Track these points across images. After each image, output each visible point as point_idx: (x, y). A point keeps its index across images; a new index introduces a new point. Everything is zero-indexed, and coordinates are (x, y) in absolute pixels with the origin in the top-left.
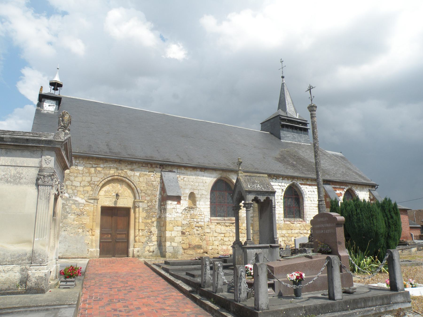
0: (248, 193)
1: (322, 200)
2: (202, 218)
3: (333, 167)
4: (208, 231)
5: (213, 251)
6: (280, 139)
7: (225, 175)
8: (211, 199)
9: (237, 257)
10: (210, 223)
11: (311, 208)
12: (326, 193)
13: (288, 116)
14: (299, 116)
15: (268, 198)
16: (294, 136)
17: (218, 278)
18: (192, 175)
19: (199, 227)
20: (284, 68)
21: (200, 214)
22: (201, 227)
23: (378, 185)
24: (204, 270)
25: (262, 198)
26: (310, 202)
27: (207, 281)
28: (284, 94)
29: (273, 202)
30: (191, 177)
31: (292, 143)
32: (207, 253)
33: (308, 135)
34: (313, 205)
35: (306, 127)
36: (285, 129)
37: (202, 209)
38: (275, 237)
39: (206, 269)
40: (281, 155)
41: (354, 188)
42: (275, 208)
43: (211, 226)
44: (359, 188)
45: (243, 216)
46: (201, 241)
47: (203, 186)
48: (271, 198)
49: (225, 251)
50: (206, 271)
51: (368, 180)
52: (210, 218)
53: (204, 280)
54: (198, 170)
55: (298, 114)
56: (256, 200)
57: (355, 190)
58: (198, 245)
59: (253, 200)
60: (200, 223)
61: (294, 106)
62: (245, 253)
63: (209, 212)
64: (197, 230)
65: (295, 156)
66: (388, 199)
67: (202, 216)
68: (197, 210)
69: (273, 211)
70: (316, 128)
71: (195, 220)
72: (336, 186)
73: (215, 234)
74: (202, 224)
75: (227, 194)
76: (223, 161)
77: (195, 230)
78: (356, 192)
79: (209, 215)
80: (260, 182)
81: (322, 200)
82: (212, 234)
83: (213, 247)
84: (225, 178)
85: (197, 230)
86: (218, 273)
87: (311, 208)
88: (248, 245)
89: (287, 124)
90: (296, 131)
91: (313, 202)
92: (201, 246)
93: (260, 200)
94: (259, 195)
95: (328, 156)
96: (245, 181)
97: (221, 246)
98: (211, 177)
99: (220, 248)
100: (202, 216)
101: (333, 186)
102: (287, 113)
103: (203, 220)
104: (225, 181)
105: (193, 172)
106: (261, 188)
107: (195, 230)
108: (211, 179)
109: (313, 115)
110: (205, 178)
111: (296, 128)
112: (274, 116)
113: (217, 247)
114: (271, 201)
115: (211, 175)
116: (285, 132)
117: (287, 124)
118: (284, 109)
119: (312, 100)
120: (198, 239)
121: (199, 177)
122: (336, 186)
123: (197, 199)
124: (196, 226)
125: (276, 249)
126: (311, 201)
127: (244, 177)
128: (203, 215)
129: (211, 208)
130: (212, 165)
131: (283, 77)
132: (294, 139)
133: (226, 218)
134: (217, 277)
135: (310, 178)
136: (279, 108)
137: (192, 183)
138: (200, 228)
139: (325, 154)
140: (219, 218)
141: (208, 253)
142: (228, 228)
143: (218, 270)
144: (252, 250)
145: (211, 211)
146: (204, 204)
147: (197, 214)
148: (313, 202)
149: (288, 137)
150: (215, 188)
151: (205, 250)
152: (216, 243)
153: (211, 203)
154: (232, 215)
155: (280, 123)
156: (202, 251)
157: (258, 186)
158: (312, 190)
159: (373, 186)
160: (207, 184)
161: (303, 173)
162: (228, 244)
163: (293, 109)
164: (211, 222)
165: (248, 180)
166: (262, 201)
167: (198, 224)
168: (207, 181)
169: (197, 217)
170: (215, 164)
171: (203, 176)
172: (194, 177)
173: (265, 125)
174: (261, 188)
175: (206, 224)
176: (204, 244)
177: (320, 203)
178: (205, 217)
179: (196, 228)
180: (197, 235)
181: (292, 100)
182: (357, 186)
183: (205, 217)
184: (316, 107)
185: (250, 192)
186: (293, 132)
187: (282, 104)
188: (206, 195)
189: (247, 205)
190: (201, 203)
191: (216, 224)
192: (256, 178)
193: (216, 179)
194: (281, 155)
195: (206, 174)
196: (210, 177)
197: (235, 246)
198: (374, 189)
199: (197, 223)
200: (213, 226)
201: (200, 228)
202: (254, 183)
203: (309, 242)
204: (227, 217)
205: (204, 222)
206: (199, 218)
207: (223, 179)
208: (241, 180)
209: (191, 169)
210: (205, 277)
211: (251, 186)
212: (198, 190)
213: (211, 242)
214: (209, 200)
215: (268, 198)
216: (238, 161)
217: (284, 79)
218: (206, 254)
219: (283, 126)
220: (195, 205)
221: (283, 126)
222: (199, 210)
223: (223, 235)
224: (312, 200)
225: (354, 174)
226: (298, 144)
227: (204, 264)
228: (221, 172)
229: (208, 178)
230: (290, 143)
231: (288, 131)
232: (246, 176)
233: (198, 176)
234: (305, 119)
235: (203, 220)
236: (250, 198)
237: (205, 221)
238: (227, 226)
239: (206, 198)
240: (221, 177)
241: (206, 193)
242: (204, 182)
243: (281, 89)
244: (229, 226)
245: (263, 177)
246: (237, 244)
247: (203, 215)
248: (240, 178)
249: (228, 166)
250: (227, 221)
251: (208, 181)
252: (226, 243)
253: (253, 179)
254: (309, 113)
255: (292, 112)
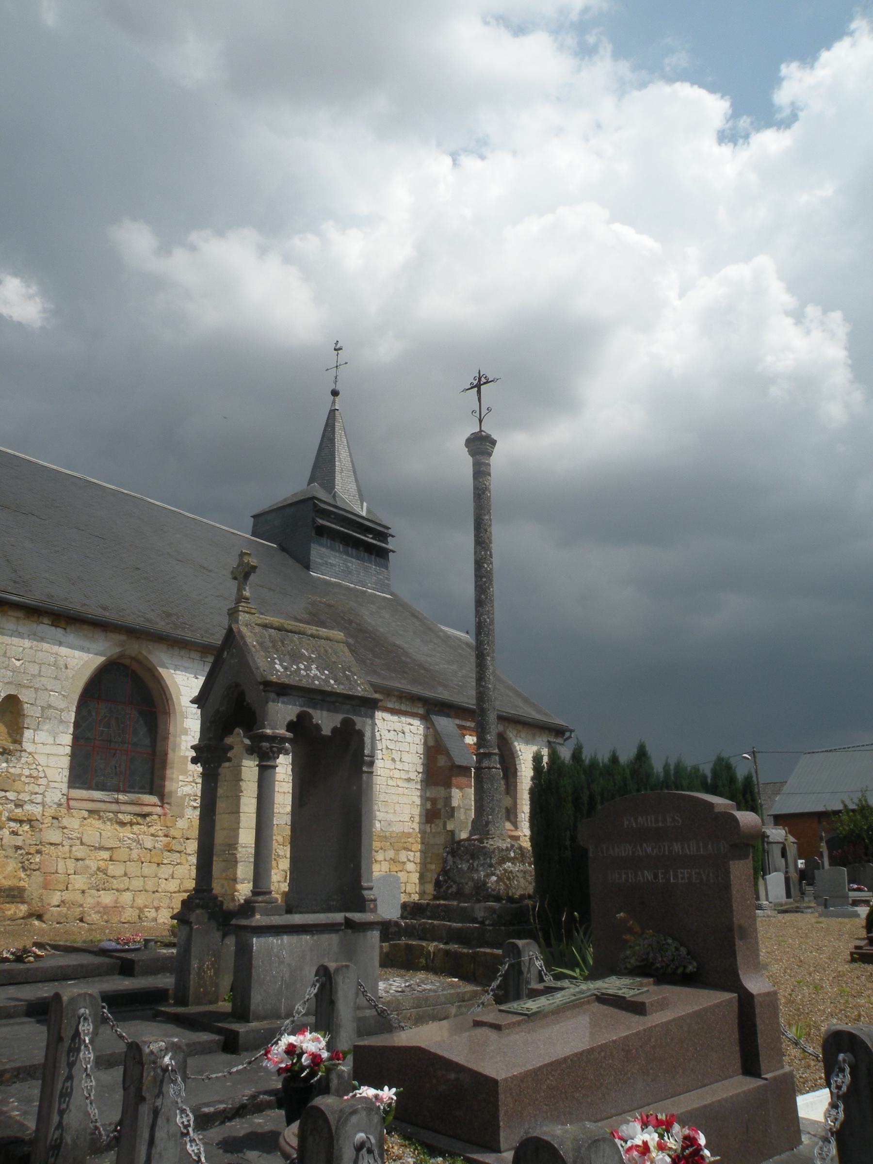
0: (273, 695)
1: (488, 755)
2: (37, 789)
3: (455, 667)
4: (54, 836)
5: (64, 910)
6: (307, 567)
7: (134, 648)
8: (76, 725)
9: (195, 964)
10: (64, 811)
11: (390, 782)
12: (436, 741)
13: (339, 504)
14: (368, 511)
15: (348, 724)
16: (348, 567)
17: (151, 1143)
18: (21, 635)
19: (21, 822)
20: (341, 368)
21: (30, 776)
22: (30, 821)
23: (571, 731)
24: (63, 1072)
25: (326, 721)
26: (389, 764)
27: (68, 1139)
28: (332, 441)
29: (367, 740)
30: (15, 640)
31: (339, 585)
32: (40, 917)
33: (387, 568)
34: (397, 774)
35: (384, 545)
36: (324, 540)
37: (42, 760)
38: (364, 884)
39: (71, 1065)
40: (310, 613)
41: (511, 734)
42: (371, 764)
43: (65, 822)
44: (523, 735)
45: (179, 794)
46: (23, 875)
47: (56, 678)
48: (359, 722)
49: (106, 910)
50: (70, 1078)
51: (546, 715)
52: (65, 791)
53: (53, 1134)
54: (46, 621)
55: (365, 504)
56: (300, 727)
57: (513, 738)
58: (11, 889)
59: (291, 726)
60: (27, 807)
61: (356, 480)
62: (244, 953)
63: (66, 772)
64: (15, 833)
65: (350, 622)
66: (672, 767)
67: (41, 781)
68: (23, 760)
69: (365, 777)
70: (489, 512)
71: (11, 795)
72: (464, 723)
73: (79, 851)
74: (37, 810)
75: (135, 714)
76: (132, 604)
77: (6, 832)
78: (516, 744)
79: (66, 780)
80: (319, 656)
81: (488, 755)
82: (67, 848)
83: (66, 896)
84: (132, 658)
85: (15, 833)
86: (156, 1112)
87: (390, 782)
88: (258, 919)
89: (334, 526)
90: (354, 551)
91: (399, 765)
92: (21, 890)
93: (318, 727)
94: (314, 707)
95: (438, 637)
96: (261, 644)
97: (94, 892)
98: (88, 651)
99: (89, 901)
100: (41, 781)
101: (458, 722)
102: (334, 496)
103: (39, 799)
104: (134, 672)
105: (26, 626)
106: (326, 681)
107: (6, 832)
108: (86, 656)
109: (483, 468)
110: (64, 651)
111: (357, 544)
112: (295, 500)
113: (79, 897)
114: (361, 734)
115: (87, 644)
116: (324, 550)
117: (334, 526)
118: (329, 483)
119: (481, 421)
120: (12, 865)
121: (46, 646)
122: (464, 723)
123: (27, 722)
124: (10, 819)
125: (369, 933)
126: (393, 760)
127: (257, 629)
128: (43, 781)
129: (73, 756)
130: (93, 610)
131: (335, 393)
132: (347, 572)
133: (121, 797)
134: (146, 1135)
135: (399, 690)
136: (311, 481)
137: (18, 663)
138: (26, 827)
139: (430, 629)
140: (97, 795)
141: (46, 917)
142: (125, 833)
143: (160, 1093)
144: (273, 941)
145: (72, 768)
146: (51, 740)
147: (20, 775)
148: (399, 765)
149: (332, 567)
150: (95, 691)
151: (36, 906)
152: (79, 882)
153: (76, 738)
154: (143, 787)
155: (314, 521)
156: (24, 908)
157: (314, 672)
158: (398, 727)
159: (559, 732)
160: (70, 673)
161: (375, 672)
162: (122, 886)
163: (352, 487)
164: (69, 808)
165: (273, 641)
166: (326, 731)
167: (19, 810)
168: (72, 663)
169: (18, 785)
170: (105, 609)
171: (60, 644)
172: (27, 643)
173: (262, 523)
174: (326, 681)
175: (50, 812)
176: (31, 884)
177: (485, 764)
178: (47, 786)
179: (12, 824)
180: (11, 852)
181: (352, 462)
182: (520, 727)
183: (47, 786)
184: (493, 443)
185: (283, 690)
186: (347, 554)
187: (324, 465)
188: (62, 711)
189: (265, 744)
190: (42, 736)
191: (86, 814)
192: (305, 639)
193: (101, 659)
194: (310, 613)
195: (71, 638)
196: (82, 649)
197: (193, 917)
198: (560, 740)
199: (17, 806)
200: (72, 823)
201: (26, 827)
202: (296, 657)
203: (436, 898)
204: (125, 791)
205: (43, 804)
206: (27, 788)
207: (127, 662)
208: (249, 640)
209: (20, 614)
210: (61, 1113)
211: (286, 668)
212: (36, 689)
213: (61, 877)
214: (71, 730)
215: (348, 724)
216: (241, 563)
217: (337, 399)
218: (36, 923)
219: (321, 531)
220: (18, 741)
221: (321, 531)
222: (30, 760)
223: (106, 855)
224: (397, 759)
225: (511, 694)
226: (358, 590)
227: (67, 1034)
228: (123, 638)
229: (77, 653)
230: (335, 584)
231: (332, 548)
232: (265, 626)
233: (42, 639)
234: (384, 523)
235: (39, 799)
236: (280, 715)
237: (48, 800)
238: (122, 824)
239: (61, 721)
240: (121, 655)
241: (62, 705)
242: (61, 663)
243: (327, 425)
244: (131, 824)
245: (328, 639)
246: (205, 906)
247: (43, 781)
248: (244, 629)
249: (148, 620)
250: (124, 808)
251: (76, 660)
252: (115, 884)
253: (292, 641)
254: (469, 460)
255: (347, 492)
